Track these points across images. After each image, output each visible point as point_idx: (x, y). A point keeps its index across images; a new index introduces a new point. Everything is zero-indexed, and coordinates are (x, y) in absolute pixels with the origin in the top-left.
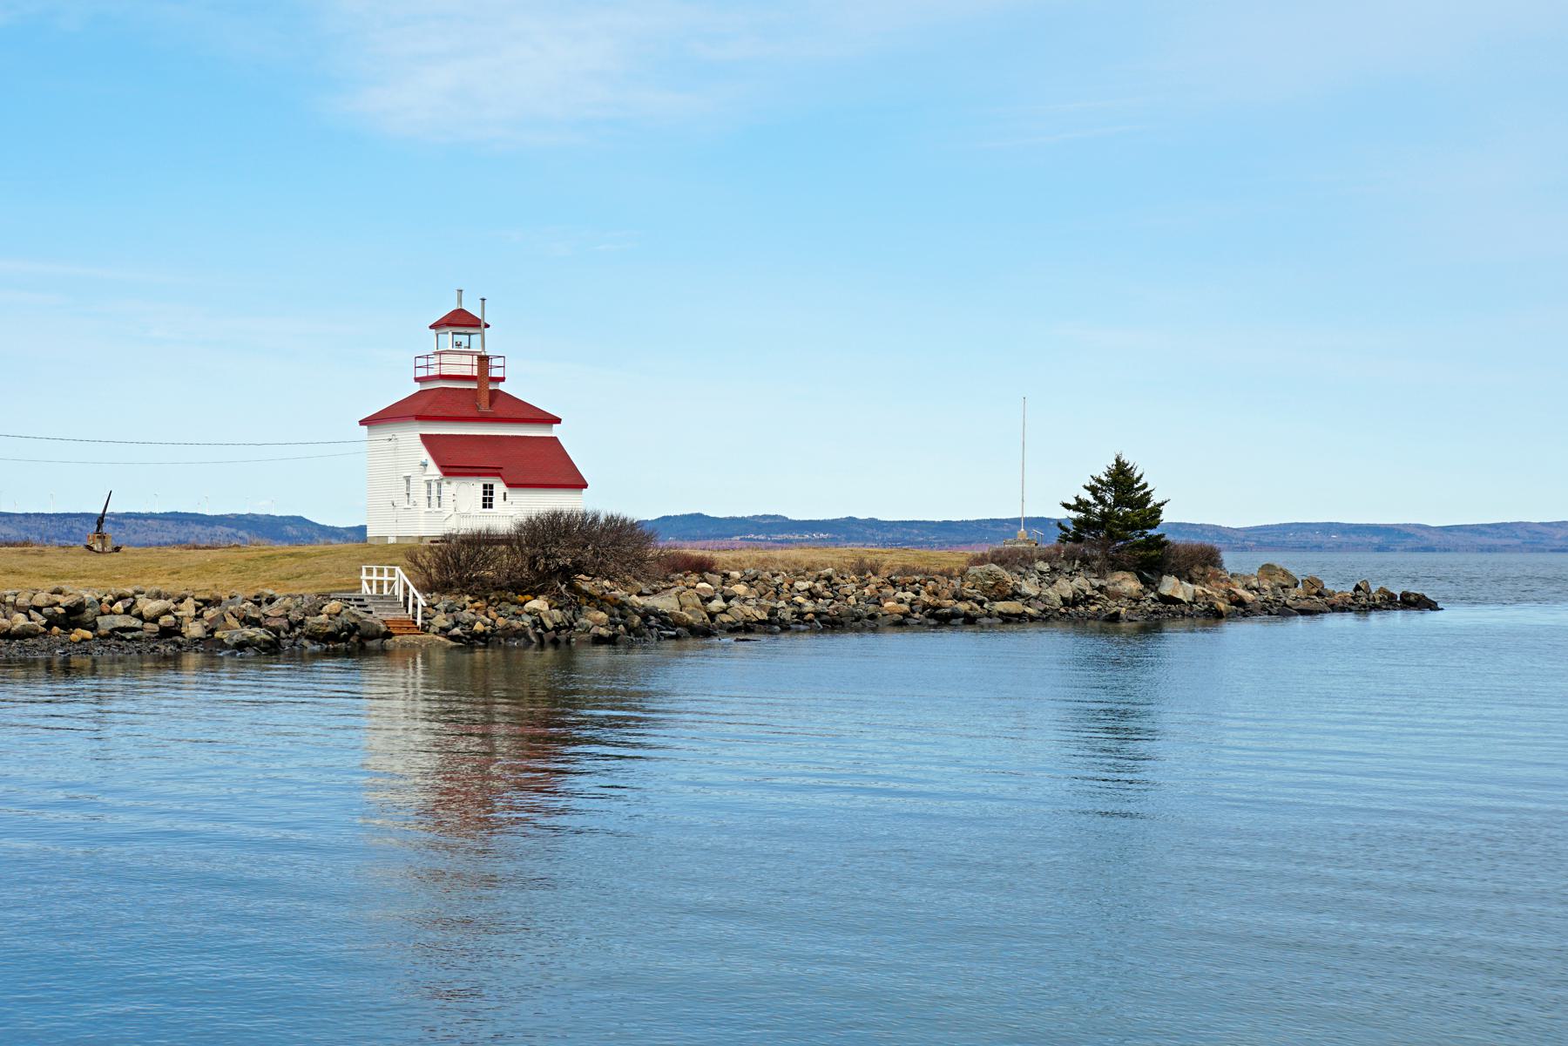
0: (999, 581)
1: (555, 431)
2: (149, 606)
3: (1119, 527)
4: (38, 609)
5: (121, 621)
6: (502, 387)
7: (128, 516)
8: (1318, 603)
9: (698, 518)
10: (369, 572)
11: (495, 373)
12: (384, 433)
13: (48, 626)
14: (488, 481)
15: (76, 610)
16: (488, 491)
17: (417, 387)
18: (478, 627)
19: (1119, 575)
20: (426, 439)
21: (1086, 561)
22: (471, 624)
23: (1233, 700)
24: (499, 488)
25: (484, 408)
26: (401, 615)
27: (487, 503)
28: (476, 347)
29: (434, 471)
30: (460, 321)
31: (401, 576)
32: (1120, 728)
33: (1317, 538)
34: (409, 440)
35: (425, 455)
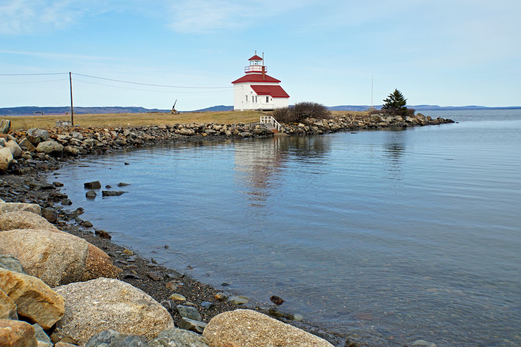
0: (379, 118)
1: (279, 84)
2: (217, 127)
3: (396, 105)
4: (192, 128)
5: (211, 131)
6: (266, 74)
7: (107, 107)
8: (430, 122)
9: (222, 107)
10: (263, 118)
11: (265, 71)
12: (239, 86)
13: (196, 132)
14: (267, 96)
15: (201, 128)
16: (267, 98)
17: (246, 74)
18: (291, 131)
19: (398, 116)
20: (251, 86)
21: (390, 113)
22: (289, 130)
23: (419, 143)
24: (270, 97)
25: (264, 79)
26: (274, 128)
27: (267, 101)
28: (262, 65)
29: (254, 94)
30: (256, 58)
31: (272, 119)
32: (396, 149)
33: (82, 111)
34: (247, 87)
35: (252, 90)
